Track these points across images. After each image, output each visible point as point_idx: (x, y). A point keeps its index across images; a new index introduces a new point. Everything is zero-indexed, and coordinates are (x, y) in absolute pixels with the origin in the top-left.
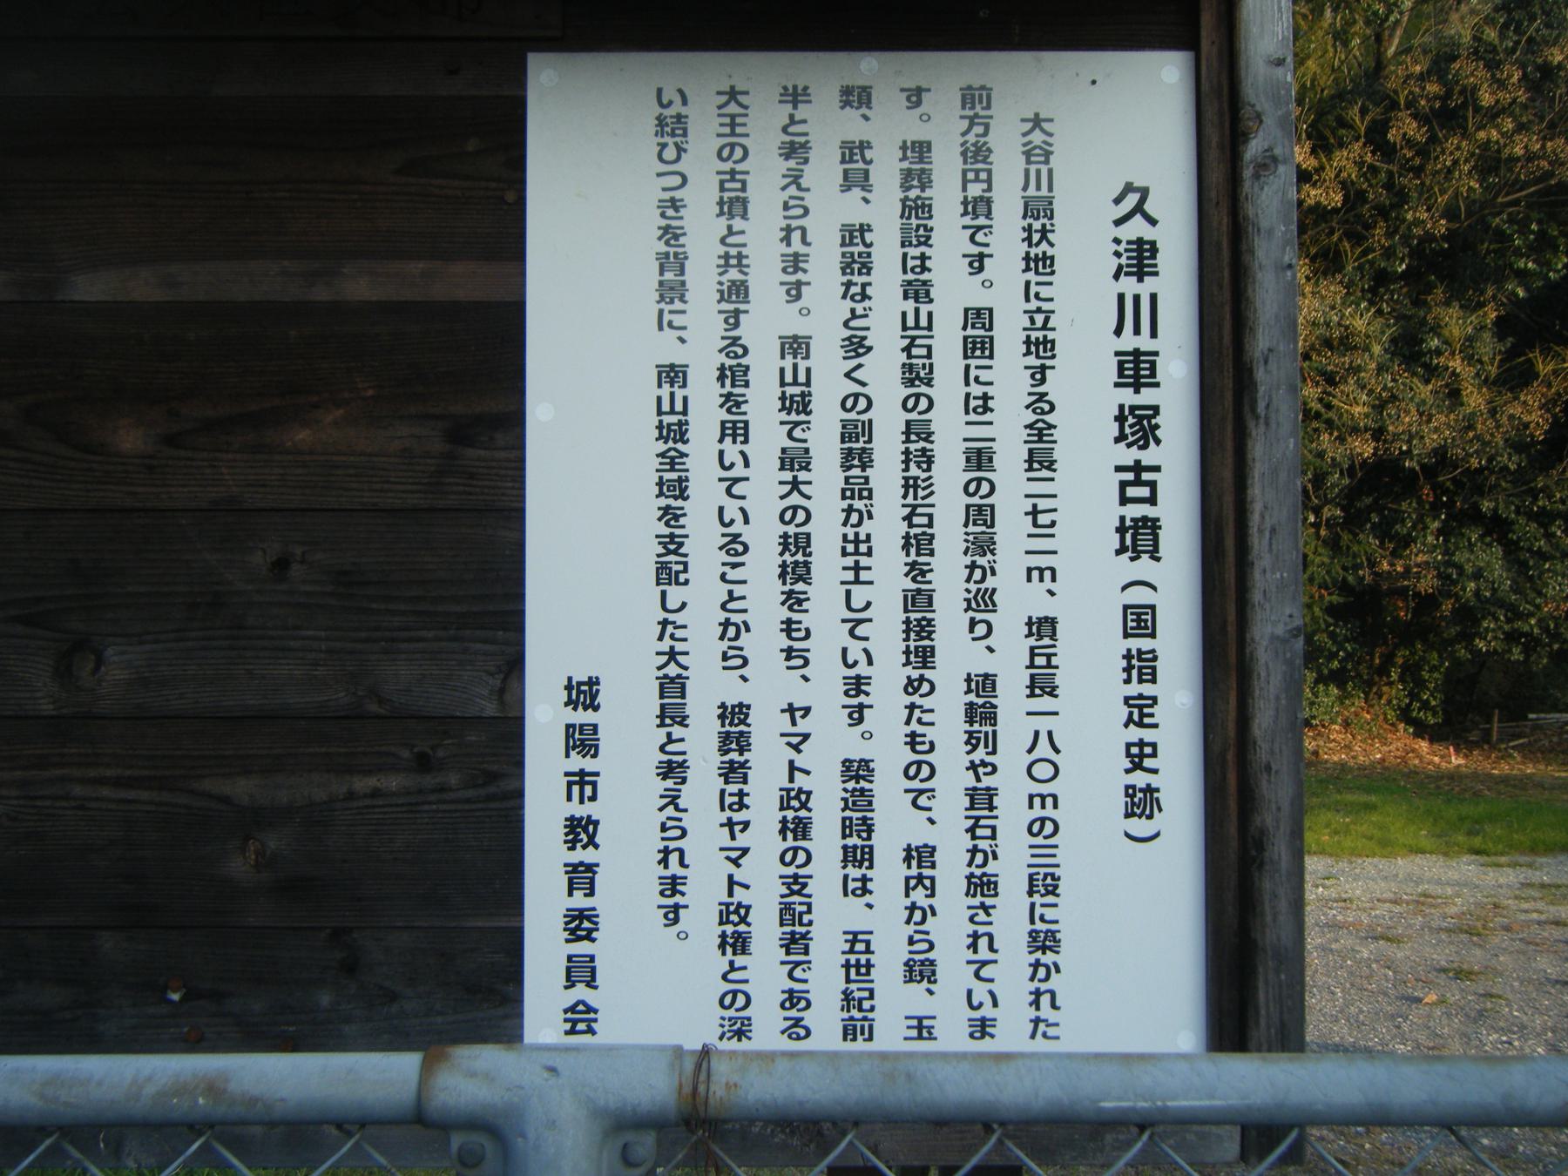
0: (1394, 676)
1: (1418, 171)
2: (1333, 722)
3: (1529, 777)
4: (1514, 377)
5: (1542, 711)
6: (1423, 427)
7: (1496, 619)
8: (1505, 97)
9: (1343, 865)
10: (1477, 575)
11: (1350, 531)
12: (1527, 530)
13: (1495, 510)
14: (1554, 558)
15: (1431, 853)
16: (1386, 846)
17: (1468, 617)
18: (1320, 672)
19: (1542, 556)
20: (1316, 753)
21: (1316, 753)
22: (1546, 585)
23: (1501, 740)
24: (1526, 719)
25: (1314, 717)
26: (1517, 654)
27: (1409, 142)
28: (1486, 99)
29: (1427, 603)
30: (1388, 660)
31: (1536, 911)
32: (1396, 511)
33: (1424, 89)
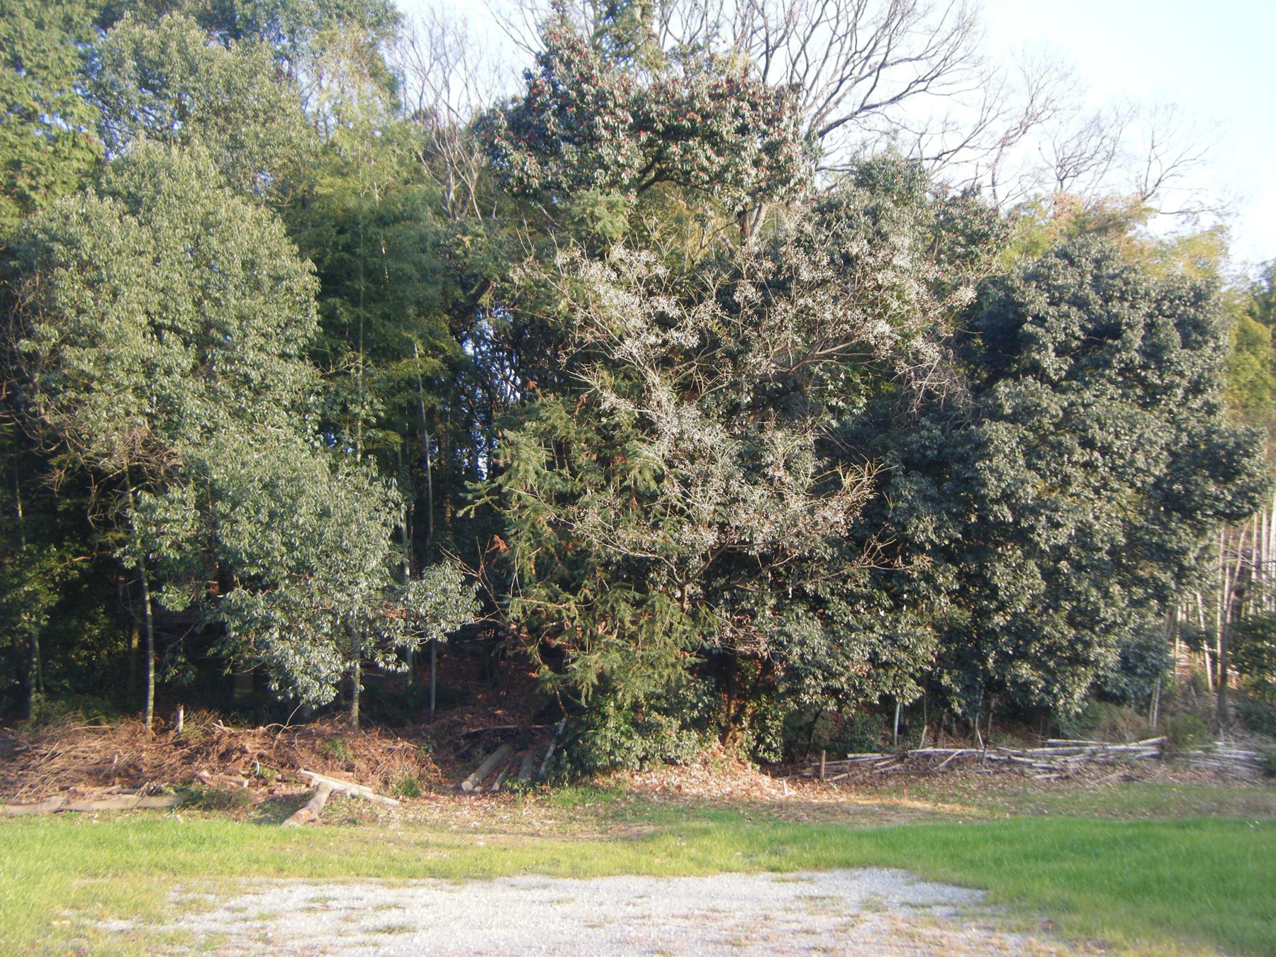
0: (745, 724)
1: (756, 326)
2: (693, 760)
3: (838, 805)
4: (825, 487)
5: (860, 752)
6: (759, 524)
7: (816, 678)
8: (818, 276)
9: (662, 884)
10: (802, 643)
11: (708, 606)
12: (838, 607)
13: (815, 591)
14: (858, 630)
15: (737, 871)
16: (702, 866)
17: (794, 674)
18: (684, 721)
19: (850, 628)
20: (679, 787)
21: (679, 787)
22: (852, 650)
23: (827, 776)
24: (846, 757)
25: (678, 757)
26: (832, 706)
27: (751, 304)
28: (805, 275)
29: (767, 666)
30: (741, 709)
31: (798, 921)
32: (743, 590)
33: (761, 264)
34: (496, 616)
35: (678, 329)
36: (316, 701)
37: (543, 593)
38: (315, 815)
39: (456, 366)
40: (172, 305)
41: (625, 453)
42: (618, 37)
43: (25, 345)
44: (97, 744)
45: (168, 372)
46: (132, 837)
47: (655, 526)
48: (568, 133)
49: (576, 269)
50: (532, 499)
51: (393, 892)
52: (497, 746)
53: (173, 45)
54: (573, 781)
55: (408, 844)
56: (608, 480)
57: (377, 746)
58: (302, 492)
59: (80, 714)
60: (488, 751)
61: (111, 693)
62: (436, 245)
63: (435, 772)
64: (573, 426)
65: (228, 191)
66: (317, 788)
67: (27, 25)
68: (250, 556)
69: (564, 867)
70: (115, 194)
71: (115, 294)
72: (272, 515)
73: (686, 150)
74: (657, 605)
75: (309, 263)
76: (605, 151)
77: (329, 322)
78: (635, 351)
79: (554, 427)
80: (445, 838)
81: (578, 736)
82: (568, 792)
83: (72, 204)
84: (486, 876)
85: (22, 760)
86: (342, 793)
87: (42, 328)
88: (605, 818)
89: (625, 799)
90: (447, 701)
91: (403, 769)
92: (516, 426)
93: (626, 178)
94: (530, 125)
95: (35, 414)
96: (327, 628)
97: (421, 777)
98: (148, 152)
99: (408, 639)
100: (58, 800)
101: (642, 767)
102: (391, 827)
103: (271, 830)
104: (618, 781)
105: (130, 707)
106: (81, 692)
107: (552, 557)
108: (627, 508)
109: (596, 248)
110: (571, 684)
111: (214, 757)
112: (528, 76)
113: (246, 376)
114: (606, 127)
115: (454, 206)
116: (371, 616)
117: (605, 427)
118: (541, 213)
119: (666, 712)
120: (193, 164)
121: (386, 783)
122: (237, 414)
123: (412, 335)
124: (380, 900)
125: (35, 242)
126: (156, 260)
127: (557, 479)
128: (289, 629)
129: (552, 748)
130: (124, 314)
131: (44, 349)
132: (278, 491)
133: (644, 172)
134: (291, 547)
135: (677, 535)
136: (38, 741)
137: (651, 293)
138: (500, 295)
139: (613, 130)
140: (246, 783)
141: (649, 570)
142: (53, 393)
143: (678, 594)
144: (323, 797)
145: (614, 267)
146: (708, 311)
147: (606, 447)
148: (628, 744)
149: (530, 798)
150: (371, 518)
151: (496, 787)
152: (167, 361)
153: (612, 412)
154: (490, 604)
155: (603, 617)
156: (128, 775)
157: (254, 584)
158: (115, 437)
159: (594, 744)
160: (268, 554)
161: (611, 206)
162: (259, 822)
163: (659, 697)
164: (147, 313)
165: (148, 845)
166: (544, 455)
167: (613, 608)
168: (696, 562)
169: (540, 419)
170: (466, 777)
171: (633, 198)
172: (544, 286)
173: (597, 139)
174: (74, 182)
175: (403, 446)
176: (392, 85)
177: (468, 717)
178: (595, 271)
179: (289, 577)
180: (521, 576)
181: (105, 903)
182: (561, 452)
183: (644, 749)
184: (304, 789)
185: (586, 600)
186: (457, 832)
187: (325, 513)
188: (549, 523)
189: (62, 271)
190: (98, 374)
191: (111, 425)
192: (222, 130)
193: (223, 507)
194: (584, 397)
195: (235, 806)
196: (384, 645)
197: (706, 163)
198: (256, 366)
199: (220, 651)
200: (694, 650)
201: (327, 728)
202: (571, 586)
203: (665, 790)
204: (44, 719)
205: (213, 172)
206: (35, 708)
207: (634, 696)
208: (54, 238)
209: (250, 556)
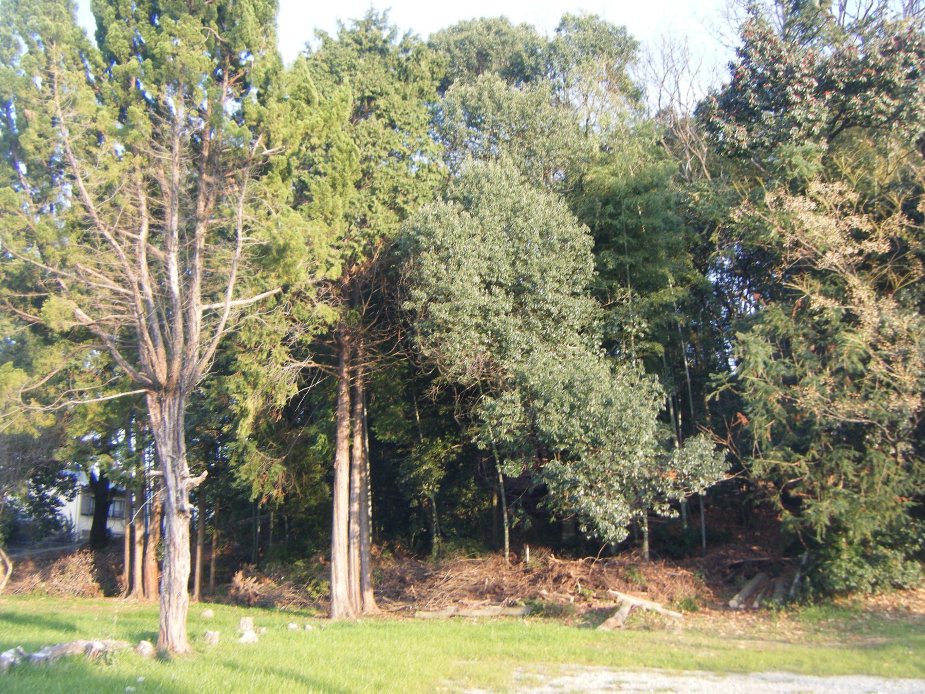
18: (907, 553)
20: (908, 608)
21: (908, 608)
25: (905, 583)
34: (745, 474)
35: (871, 240)
36: (614, 540)
37: (779, 454)
38: (620, 623)
39: (700, 292)
40: (495, 267)
41: (835, 342)
42: (803, 25)
43: (407, 305)
44: (475, 571)
45: (497, 314)
46: (493, 634)
47: (866, 398)
48: (766, 104)
49: (781, 205)
50: (762, 384)
51: (670, 679)
52: (755, 573)
53: (486, 93)
54: (817, 601)
55: (685, 645)
56: (824, 366)
57: (663, 573)
58: (591, 389)
59: (463, 551)
60: (749, 577)
61: (482, 537)
62: (678, 203)
63: (708, 593)
64: (792, 325)
65: (527, 185)
66: (621, 603)
67: (397, 98)
68: (559, 436)
69: (805, 667)
70: (455, 199)
71: (459, 265)
72: (572, 407)
73: (865, 100)
74: (875, 461)
75: (586, 228)
76: (798, 113)
77: (601, 268)
78: (835, 261)
79: (776, 328)
80: (715, 642)
81: (818, 566)
82: (813, 610)
83: (428, 209)
84: (743, 671)
85: (429, 582)
86: (640, 608)
87: (417, 293)
88: (845, 631)
89: (861, 617)
90: (715, 540)
91: (684, 590)
92: (746, 329)
93: (816, 130)
94: (736, 102)
95: (416, 350)
96: (617, 486)
97: (697, 597)
98: (474, 168)
99: (676, 493)
100: (451, 609)
101: (874, 591)
102: (675, 633)
103: (588, 632)
104: (854, 602)
105: (495, 547)
106: (464, 536)
107: (784, 427)
108: (842, 385)
109: (798, 187)
110: (808, 524)
111: (550, 581)
112: (732, 66)
113: (548, 310)
114: (796, 93)
115: (691, 174)
116: (647, 475)
117: (818, 323)
118: (755, 167)
119: (892, 547)
120: (502, 172)
121: (671, 600)
122: (545, 338)
123: (666, 271)
124: (659, 685)
125: (409, 237)
126: (483, 240)
127: (782, 367)
128: (591, 487)
129: (798, 575)
130: (465, 277)
131: (418, 307)
132: (574, 390)
133: (832, 123)
134: (587, 429)
135: (885, 403)
136: (439, 568)
137: (846, 215)
138: (727, 235)
139: (801, 95)
140: (572, 599)
141: (865, 433)
142: (425, 334)
143: (893, 451)
144: (625, 610)
145: (813, 199)
146: (897, 223)
147: (821, 339)
148: (860, 572)
149: (783, 614)
150: (642, 405)
151: (756, 605)
152: (495, 306)
153: (822, 310)
154: (736, 466)
155: (831, 471)
156: (495, 593)
157: (565, 456)
158: (467, 361)
159: (831, 572)
160: (571, 435)
161: (806, 154)
162: (579, 627)
163: (883, 535)
164: (481, 275)
165: (504, 640)
166: (770, 350)
167: (837, 465)
168: (905, 424)
169: (764, 323)
170: (732, 597)
171: (824, 146)
172: (759, 220)
173: (788, 104)
174: (430, 196)
175: (666, 353)
176: (636, 96)
177: (731, 552)
178: (796, 203)
179: (588, 450)
180: (760, 443)
181: (470, 677)
182: (784, 347)
183: (875, 577)
184: (612, 604)
185: (814, 459)
186: (725, 638)
187: (608, 404)
188: (778, 401)
189: (425, 254)
190: (451, 320)
191: (463, 354)
192: (522, 145)
193: (538, 404)
194: (798, 302)
195: (566, 615)
196: (659, 497)
197: (883, 107)
198: (554, 303)
199: (546, 505)
200: (910, 495)
201: (626, 559)
202: (801, 448)
203: (896, 610)
204: (441, 555)
205: (516, 173)
206: (436, 547)
207: (863, 534)
208: (419, 233)
209: (559, 436)
